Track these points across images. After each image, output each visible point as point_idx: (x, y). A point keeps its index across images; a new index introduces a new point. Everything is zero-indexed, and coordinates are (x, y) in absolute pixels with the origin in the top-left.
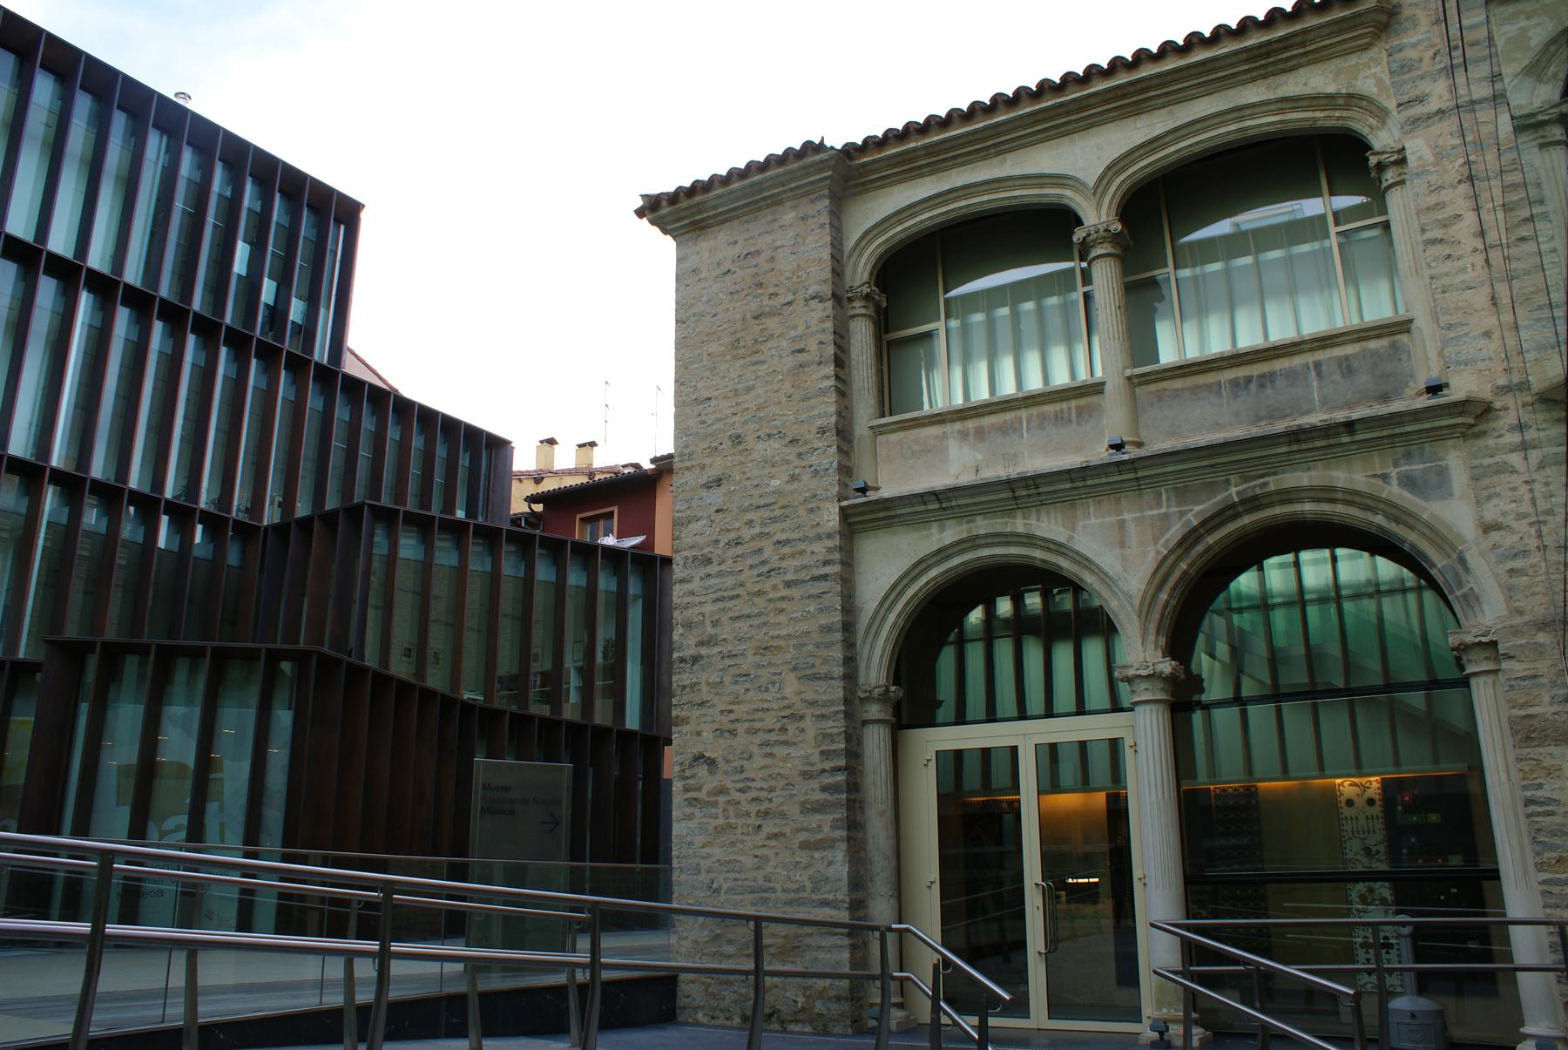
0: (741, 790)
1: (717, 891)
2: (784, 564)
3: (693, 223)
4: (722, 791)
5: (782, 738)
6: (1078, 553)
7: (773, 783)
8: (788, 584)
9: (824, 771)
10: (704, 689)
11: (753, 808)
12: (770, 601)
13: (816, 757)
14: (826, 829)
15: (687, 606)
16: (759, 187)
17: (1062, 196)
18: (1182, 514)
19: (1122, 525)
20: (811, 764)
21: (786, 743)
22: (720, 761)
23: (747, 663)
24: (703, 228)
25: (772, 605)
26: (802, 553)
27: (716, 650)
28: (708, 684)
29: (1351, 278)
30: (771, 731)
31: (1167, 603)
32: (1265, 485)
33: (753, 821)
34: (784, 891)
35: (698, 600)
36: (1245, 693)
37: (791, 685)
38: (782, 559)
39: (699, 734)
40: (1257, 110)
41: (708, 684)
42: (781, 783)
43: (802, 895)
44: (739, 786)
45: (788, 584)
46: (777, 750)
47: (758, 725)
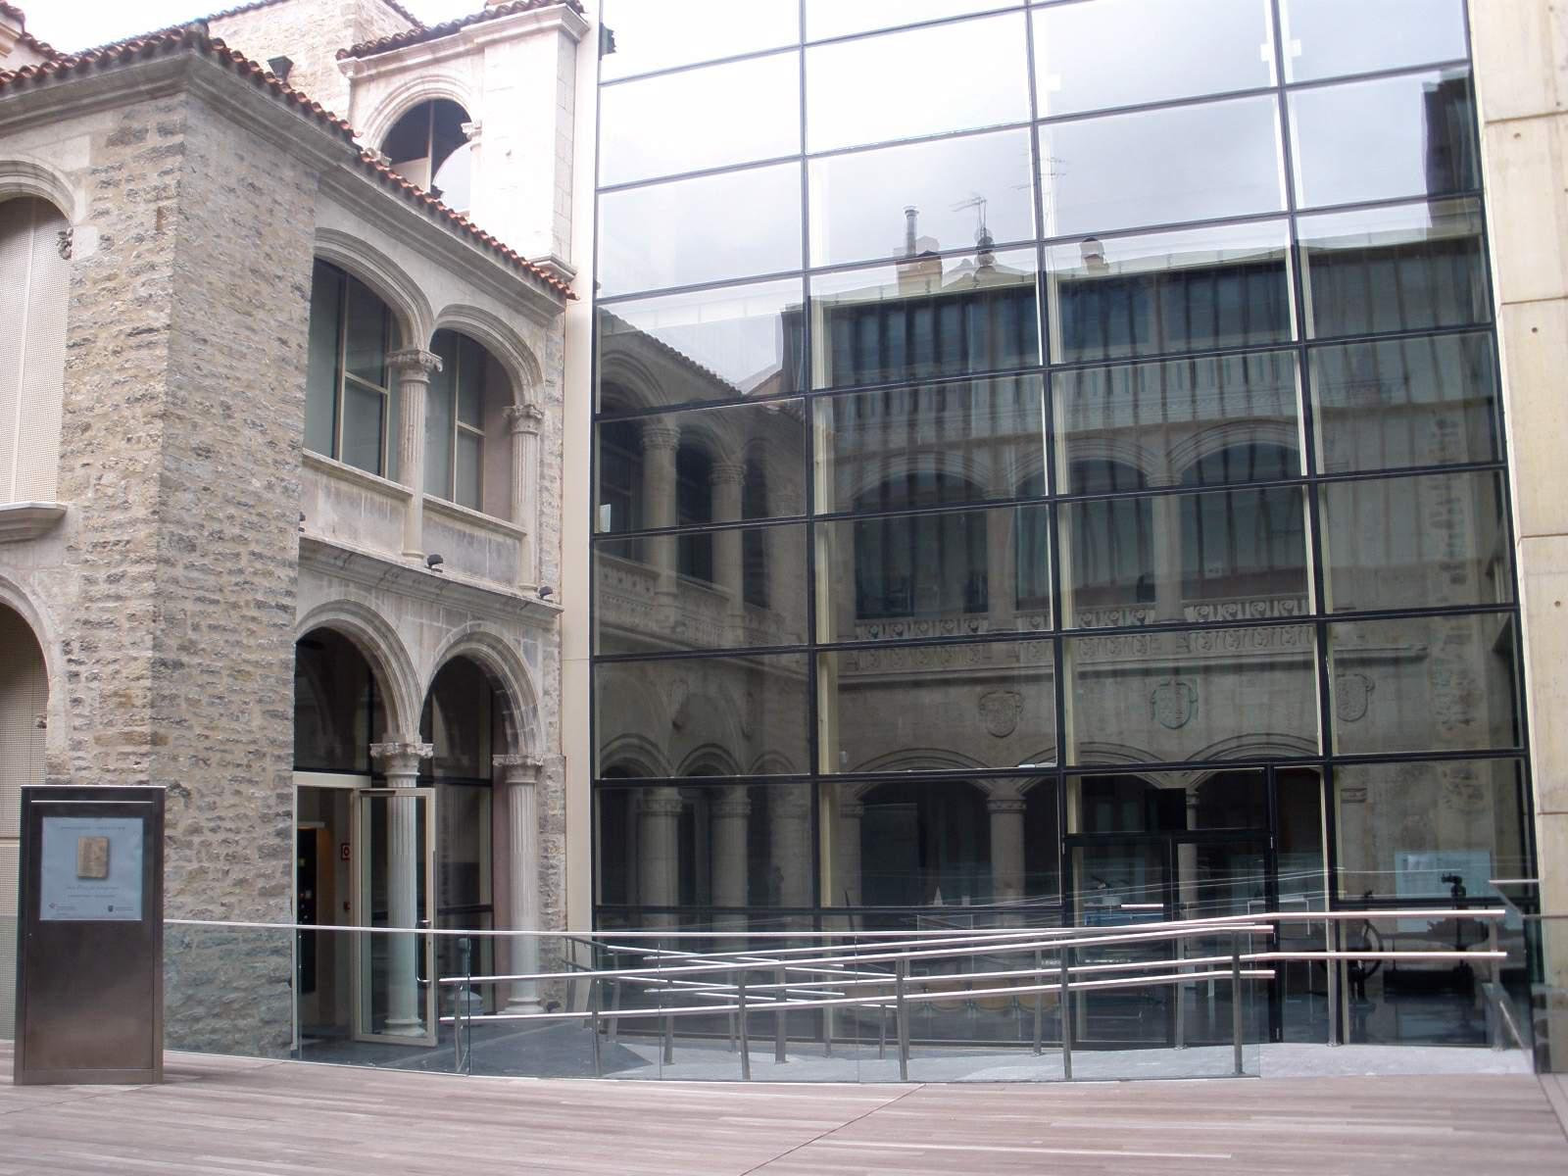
0: (213, 830)
1: (188, 946)
2: (256, 580)
3: (215, 98)
4: (196, 830)
5: (247, 775)
6: (398, 641)
7: (240, 824)
8: (260, 605)
9: (278, 815)
10: (184, 705)
11: (223, 851)
12: (243, 617)
13: (273, 801)
14: (278, 875)
16: (290, 124)
17: (410, 307)
18: (448, 631)
19: (422, 625)
20: (269, 807)
21: (250, 781)
22: (195, 795)
23: (223, 684)
24: (216, 109)
25: (244, 624)
27: (197, 660)
28: (187, 699)
30: (239, 765)
32: (479, 625)
33: (222, 865)
34: (245, 941)
35: (181, 592)
37: (257, 721)
38: (255, 573)
39: (175, 758)
40: (501, 328)
41: (187, 699)
42: (245, 825)
43: (259, 944)
44: (212, 824)
45: (260, 605)
46: (243, 788)
47: (229, 757)
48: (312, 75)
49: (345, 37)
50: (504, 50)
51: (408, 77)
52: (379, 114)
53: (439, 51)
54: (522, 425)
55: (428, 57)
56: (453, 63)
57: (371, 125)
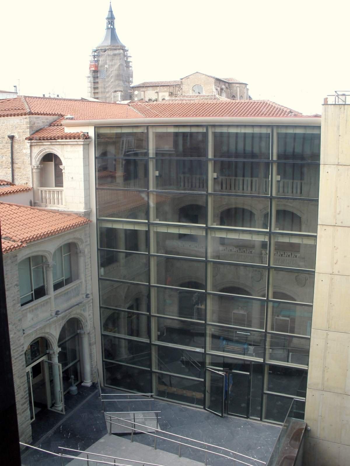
15: (344, 109)
26: (18, 351)
29: (134, 186)
31: (52, 341)
36: (332, 335)
48: (20, 140)
49: (27, 131)
50: (69, 147)
51: (45, 147)
52: (38, 155)
53: (52, 143)
54: (80, 255)
55: (49, 144)
56: (56, 146)
57: (36, 158)
